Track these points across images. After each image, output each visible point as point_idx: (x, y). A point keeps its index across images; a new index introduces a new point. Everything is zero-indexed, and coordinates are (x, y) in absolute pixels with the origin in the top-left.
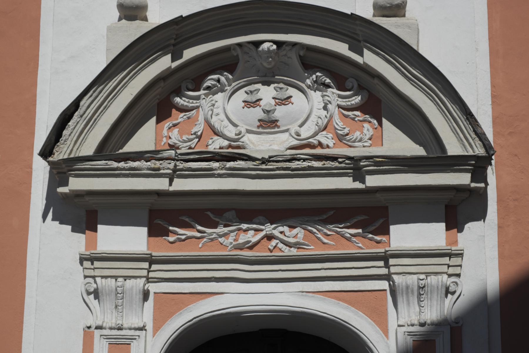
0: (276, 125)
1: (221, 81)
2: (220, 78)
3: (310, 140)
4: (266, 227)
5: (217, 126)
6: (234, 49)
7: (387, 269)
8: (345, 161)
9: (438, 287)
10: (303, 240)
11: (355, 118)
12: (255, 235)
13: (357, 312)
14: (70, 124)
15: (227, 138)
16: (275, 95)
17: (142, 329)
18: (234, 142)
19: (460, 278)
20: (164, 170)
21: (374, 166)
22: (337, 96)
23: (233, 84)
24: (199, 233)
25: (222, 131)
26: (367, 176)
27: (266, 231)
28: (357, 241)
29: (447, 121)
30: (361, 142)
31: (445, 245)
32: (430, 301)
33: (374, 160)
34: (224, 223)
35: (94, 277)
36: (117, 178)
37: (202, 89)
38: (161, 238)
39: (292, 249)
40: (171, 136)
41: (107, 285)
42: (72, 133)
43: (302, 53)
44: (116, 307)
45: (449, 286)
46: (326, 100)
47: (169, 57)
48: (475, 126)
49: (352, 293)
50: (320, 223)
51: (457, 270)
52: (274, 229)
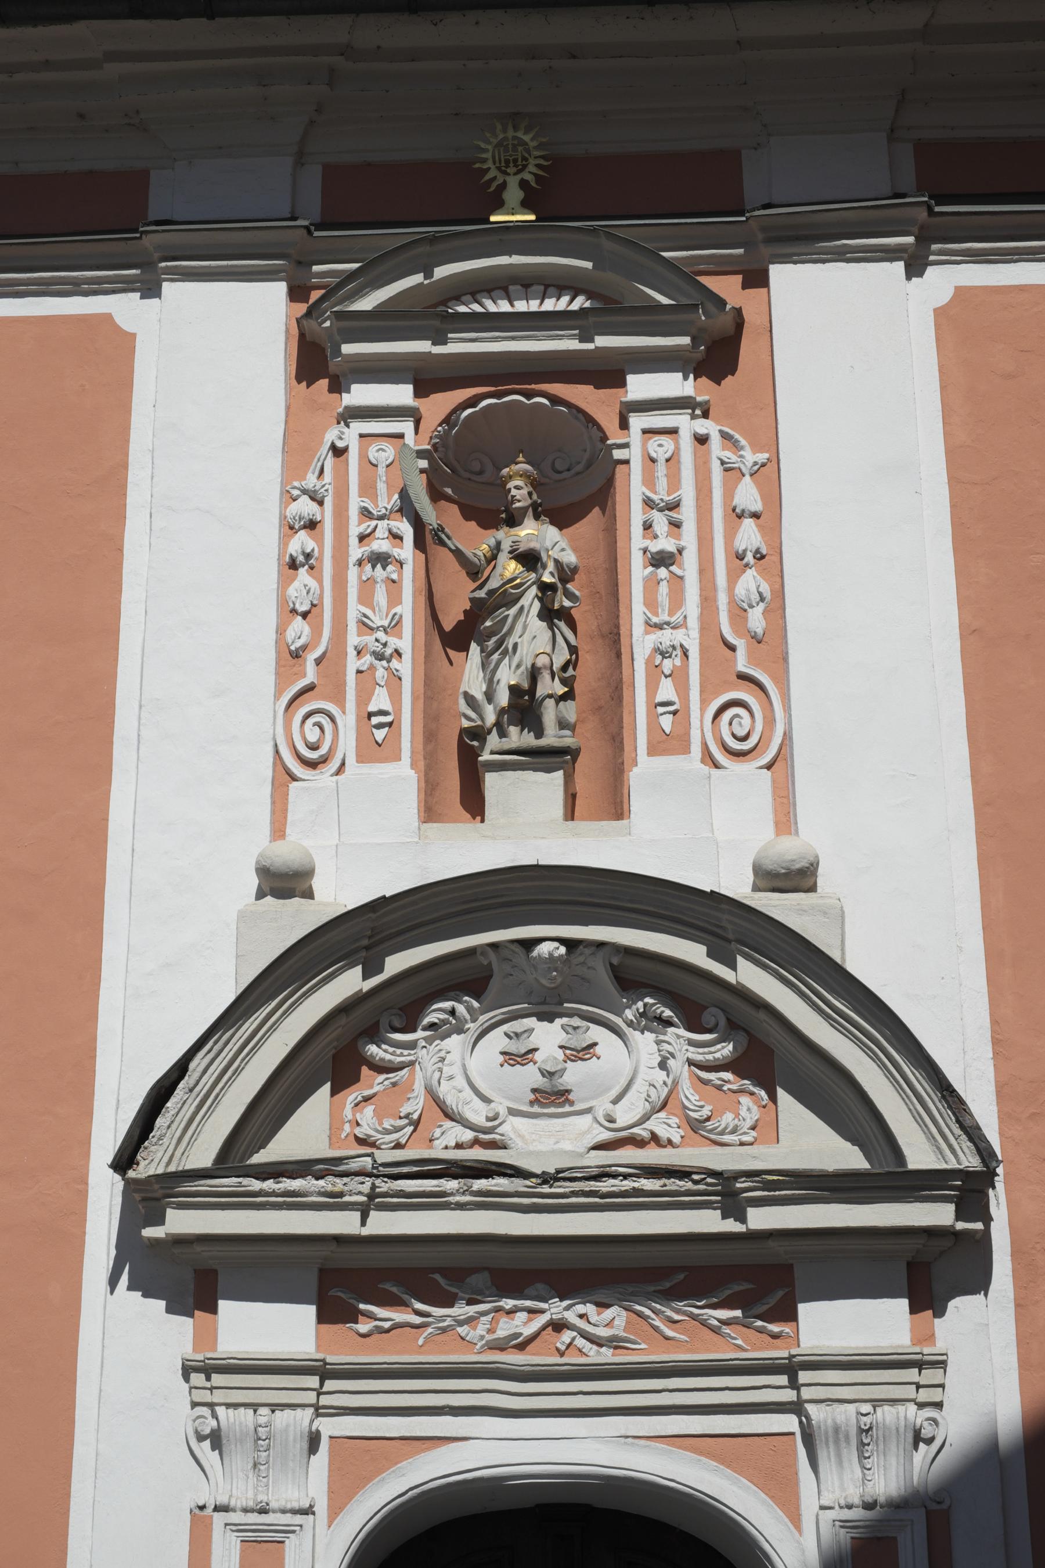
0: (567, 1100)
1: (457, 1014)
2: (455, 1006)
3: (635, 1130)
4: (551, 1306)
5: (451, 1101)
6: (482, 954)
7: (795, 1392)
8: (705, 1178)
9: (897, 1429)
10: (624, 1331)
11: (723, 1085)
12: (530, 1320)
13: (736, 1478)
14: (169, 1104)
15: (472, 1126)
16: (563, 1040)
17: (308, 1511)
18: (485, 1133)
19: (941, 1410)
20: (350, 1195)
21: (763, 1190)
22: (687, 1042)
23: (481, 1017)
24: (418, 1317)
25: (461, 1112)
26: (749, 1209)
27: (552, 1314)
28: (732, 1335)
29: (903, 1099)
30: (735, 1134)
32: (883, 1458)
33: (762, 1178)
34: (467, 1296)
35: (211, 1406)
36: (258, 1210)
37: (420, 1027)
38: (343, 1325)
39: (604, 1349)
40: (359, 1122)
41: (237, 1423)
42: (172, 1122)
43: (615, 961)
44: (255, 1465)
45: (921, 1426)
46: (664, 1052)
48: (959, 1112)
49: (726, 1438)
50: (658, 1298)
51: (935, 1395)
52: (568, 1308)
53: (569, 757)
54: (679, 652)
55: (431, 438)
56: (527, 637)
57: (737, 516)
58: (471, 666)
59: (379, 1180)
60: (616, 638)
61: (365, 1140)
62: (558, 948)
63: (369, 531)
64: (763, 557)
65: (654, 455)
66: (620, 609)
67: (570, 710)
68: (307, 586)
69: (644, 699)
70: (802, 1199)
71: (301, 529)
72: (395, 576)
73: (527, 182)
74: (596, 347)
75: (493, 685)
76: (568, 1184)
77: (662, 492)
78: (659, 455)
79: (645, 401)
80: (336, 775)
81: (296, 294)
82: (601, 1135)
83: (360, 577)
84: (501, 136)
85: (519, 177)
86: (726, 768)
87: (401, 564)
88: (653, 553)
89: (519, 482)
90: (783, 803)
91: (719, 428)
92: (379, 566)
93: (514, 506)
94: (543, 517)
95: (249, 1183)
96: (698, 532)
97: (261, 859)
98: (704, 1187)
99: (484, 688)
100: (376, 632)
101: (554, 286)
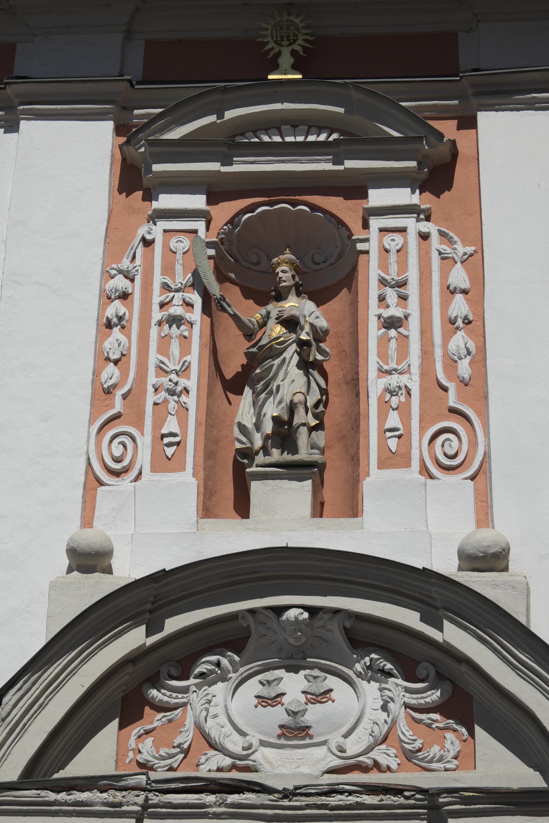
0: (307, 734)
2: (220, 659)
3: (361, 759)
5: (214, 734)
6: (243, 618)
8: (414, 795)
11: (432, 724)
15: (232, 755)
18: (241, 760)
20: (128, 806)
22: (404, 689)
23: (241, 669)
30: (441, 763)
33: (460, 794)
36: (53, 816)
37: (192, 676)
43: (348, 625)
46: (386, 697)
53: (316, 469)
54: (404, 391)
55: (218, 234)
56: (287, 381)
57: (451, 292)
58: (245, 403)
59: (152, 794)
60: (356, 382)
61: (145, 764)
62: (302, 614)
63: (168, 300)
64: (470, 322)
65: (388, 247)
66: (360, 359)
67: (320, 438)
68: (118, 340)
69: (376, 426)
70: (490, 812)
71: (115, 299)
72: (186, 334)
73: (297, 51)
74: (345, 168)
75: (261, 418)
76: (304, 798)
77: (393, 274)
78: (392, 247)
79: (382, 207)
80: (135, 482)
81: (119, 130)
82: (333, 762)
83: (159, 334)
84: (278, 19)
85: (291, 48)
86: (439, 479)
87: (192, 325)
88: (385, 318)
89: (285, 268)
90: (483, 506)
91: (438, 228)
92: (174, 326)
93: (281, 285)
94: (303, 295)
95: (47, 794)
96: (420, 303)
97: (70, 542)
98: (414, 802)
99: (254, 420)
100: (170, 375)
101: (315, 126)
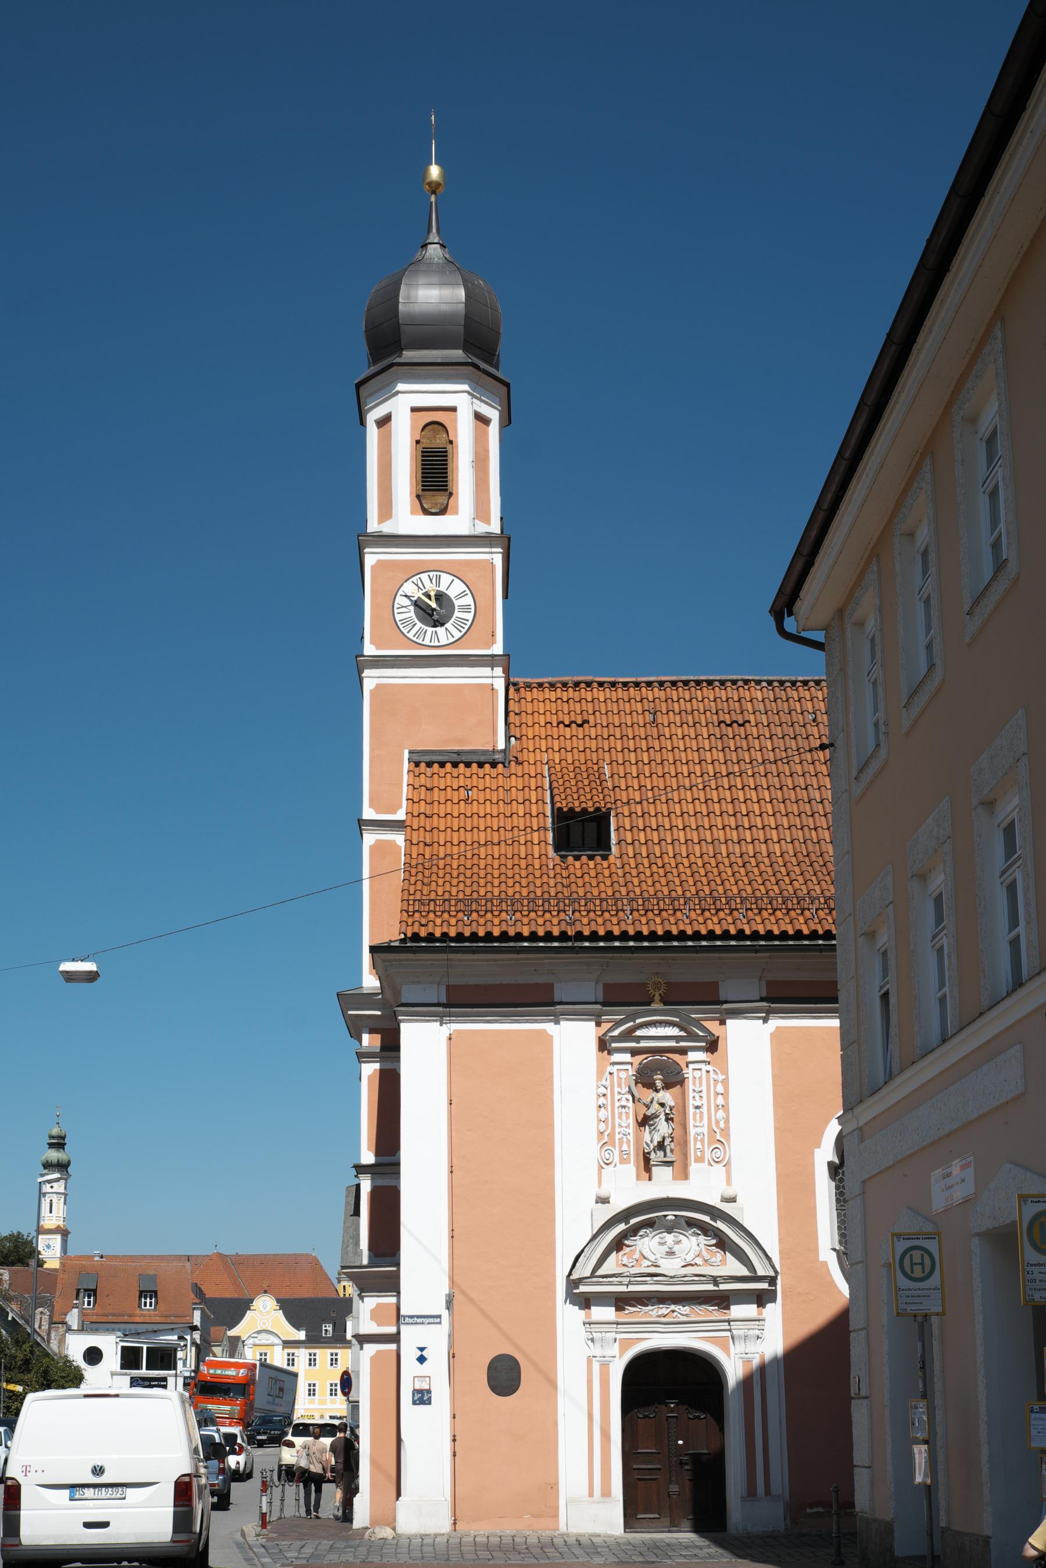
5: (646, 1255)
31: (756, 1314)
47: (624, 1224)
51: (762, 1327)
